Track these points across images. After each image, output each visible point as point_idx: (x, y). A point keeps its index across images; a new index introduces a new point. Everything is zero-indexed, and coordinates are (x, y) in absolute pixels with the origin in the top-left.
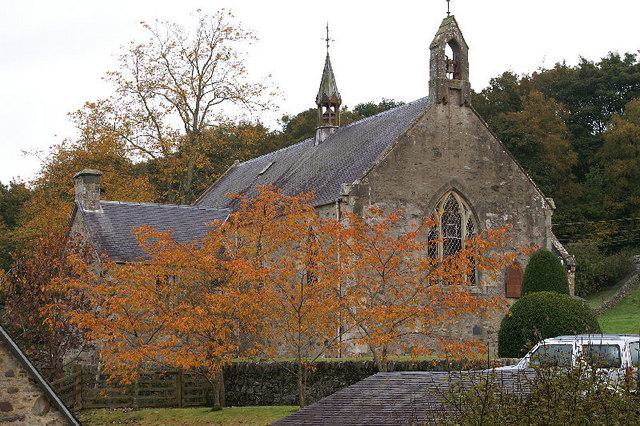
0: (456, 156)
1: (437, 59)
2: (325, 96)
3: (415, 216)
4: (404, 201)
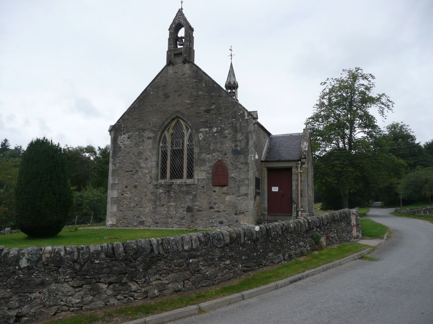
0: (180, 95)
1: (174, 39)
2: (230, 82)
3: (149, 138)
4: (144, 130)
